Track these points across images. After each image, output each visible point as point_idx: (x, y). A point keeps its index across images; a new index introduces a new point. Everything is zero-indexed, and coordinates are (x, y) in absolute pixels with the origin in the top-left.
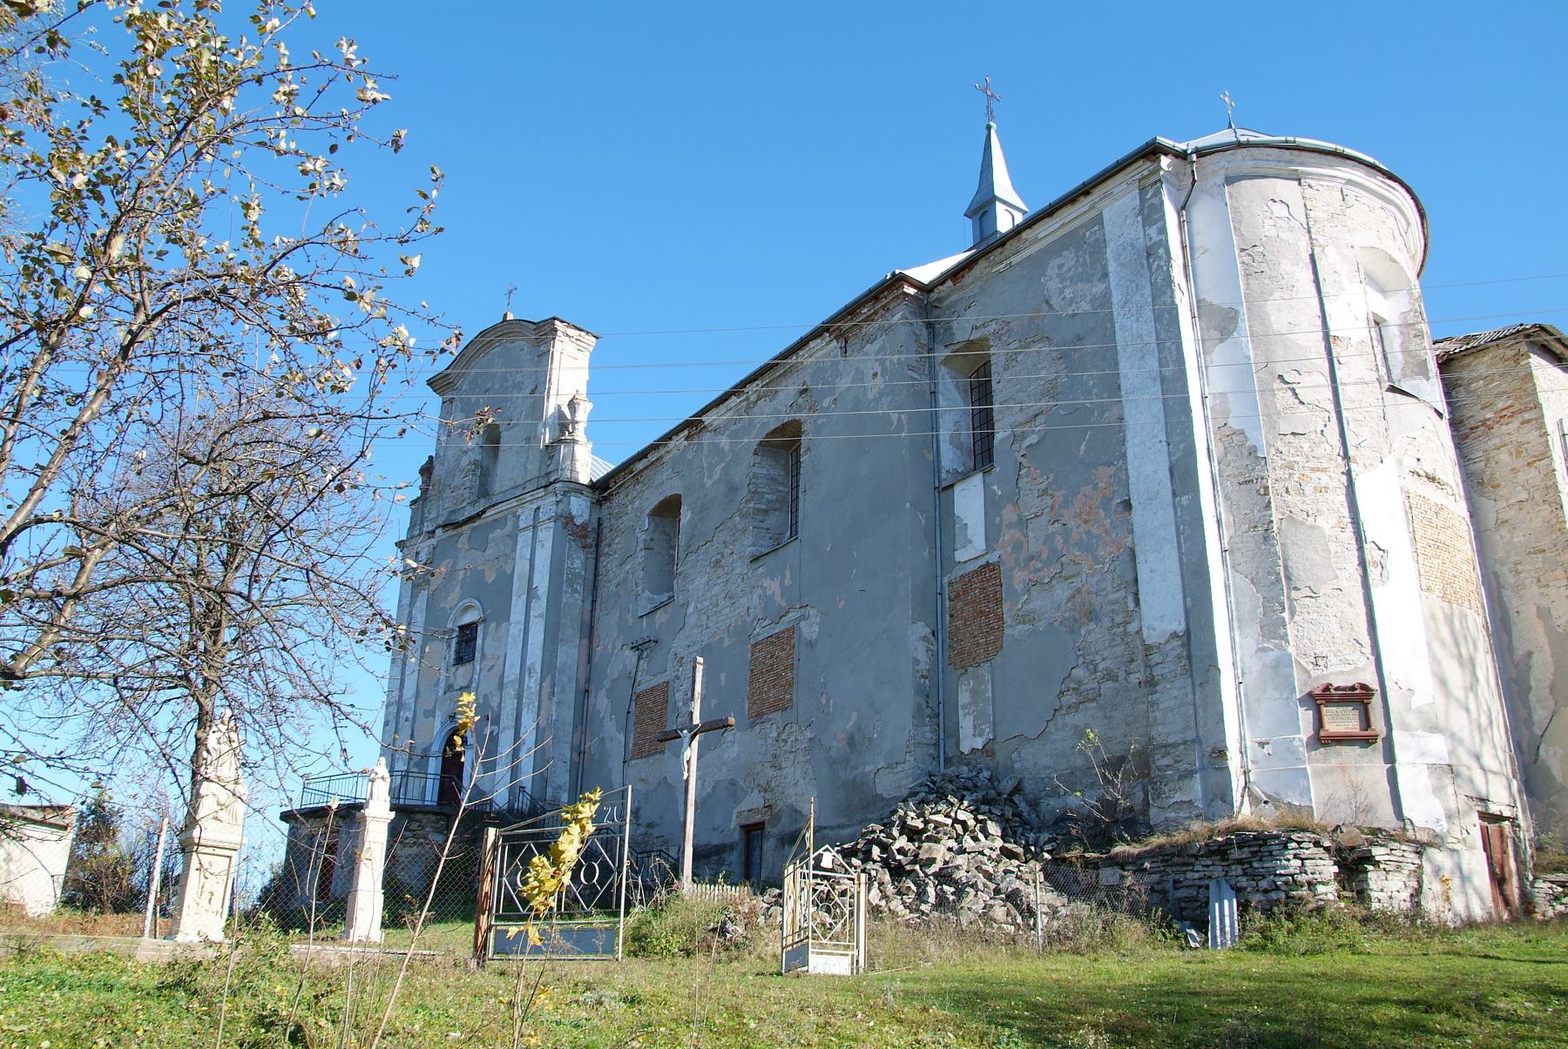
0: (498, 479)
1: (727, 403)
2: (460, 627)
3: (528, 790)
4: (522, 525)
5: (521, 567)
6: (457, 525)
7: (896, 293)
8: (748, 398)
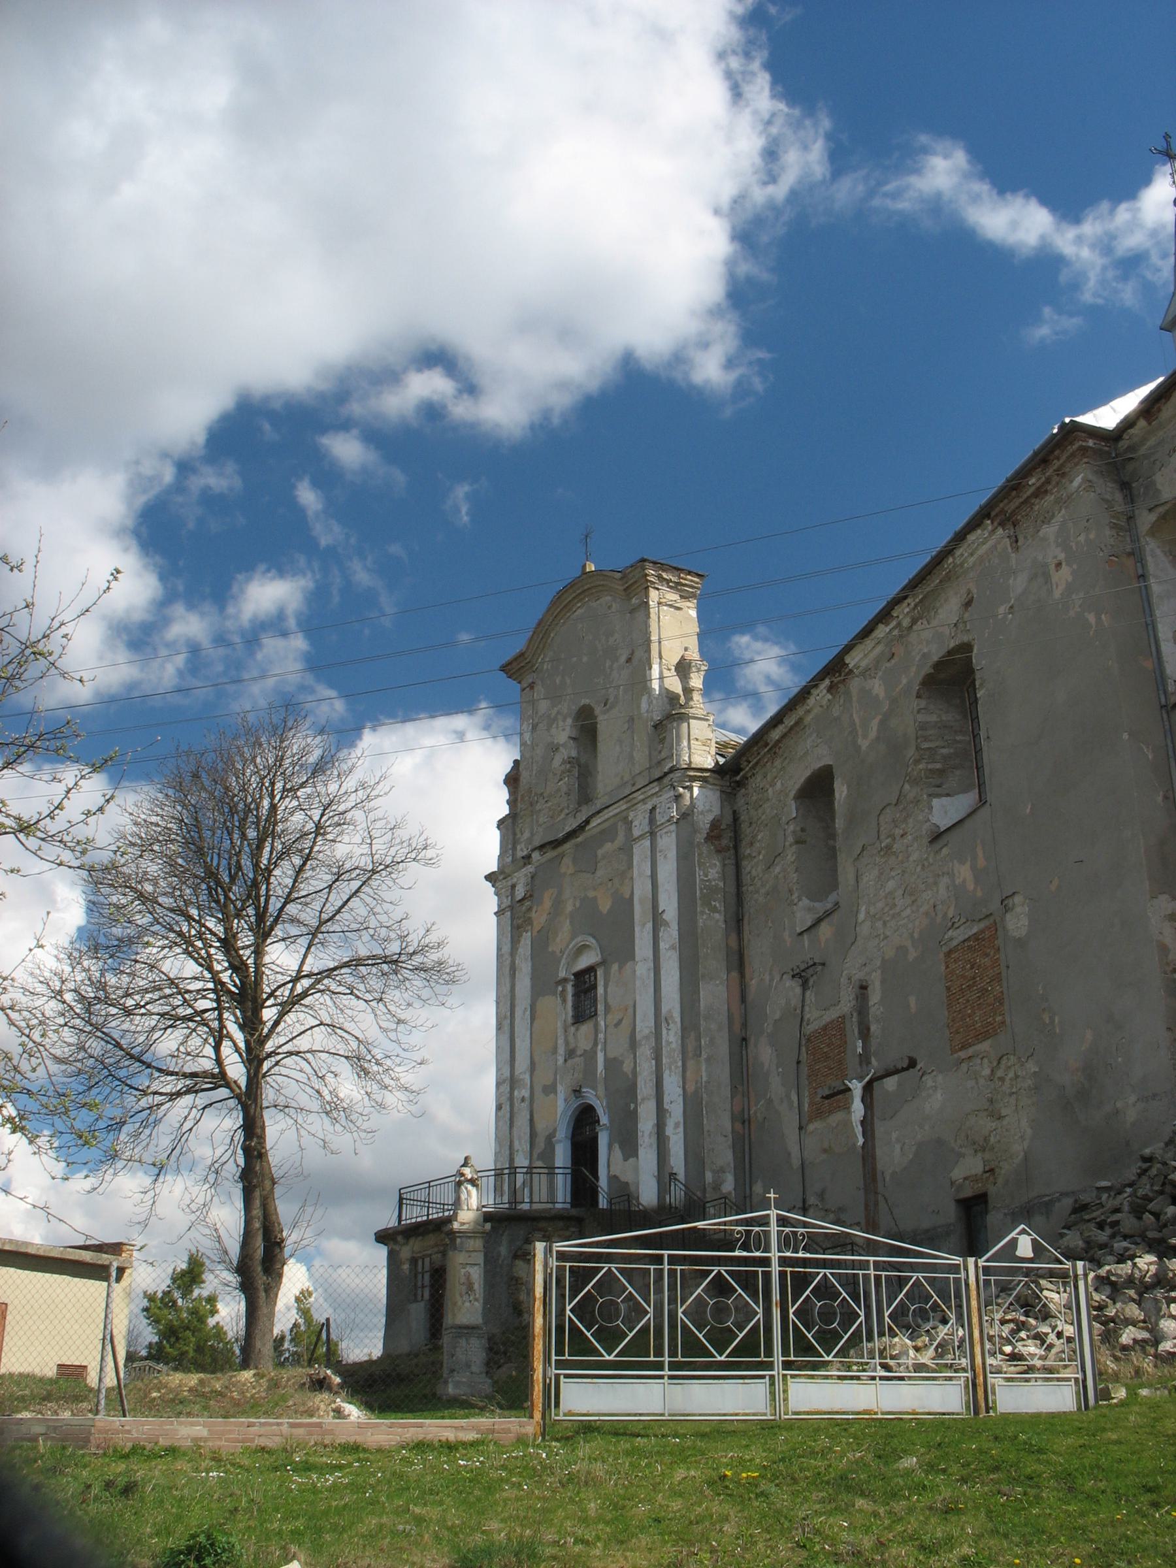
0: (600, 777)
1: (874, 635)
2: (574, 974)
3: (681, 1176)
4: (636, 832)
5: (641, 888)
6: (556, 844)
7: (1071, 449)
8: (899, 624)
